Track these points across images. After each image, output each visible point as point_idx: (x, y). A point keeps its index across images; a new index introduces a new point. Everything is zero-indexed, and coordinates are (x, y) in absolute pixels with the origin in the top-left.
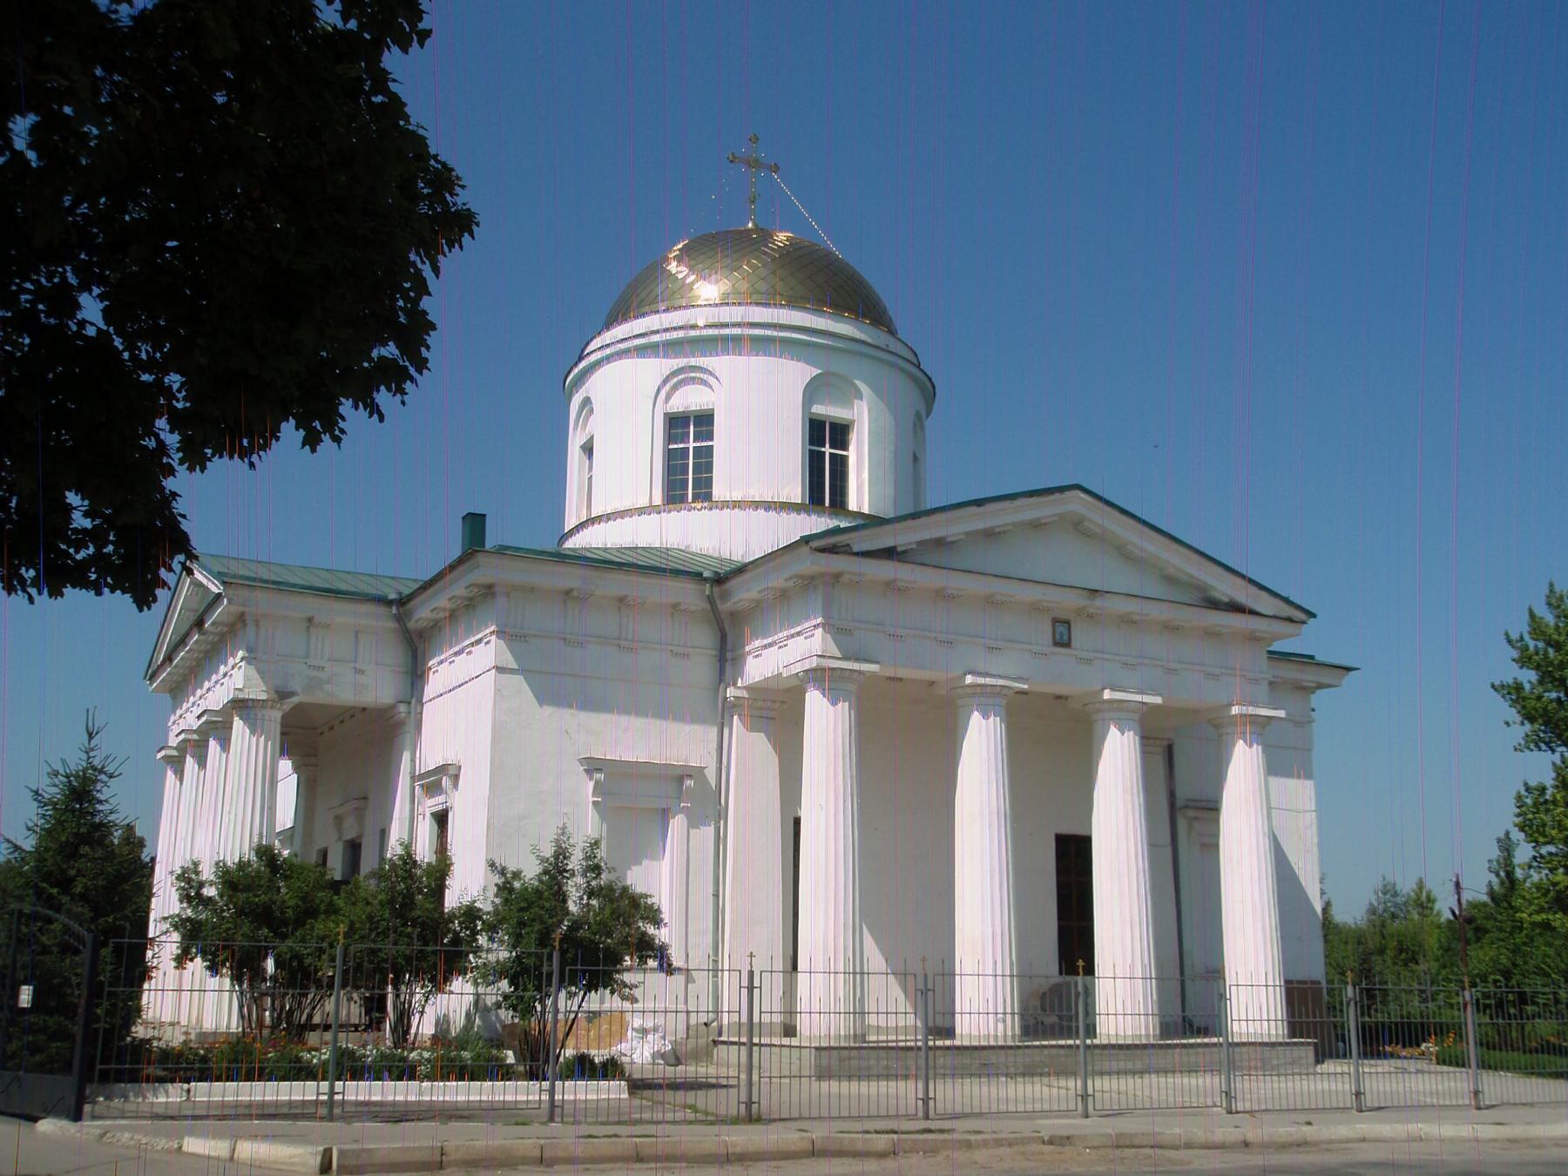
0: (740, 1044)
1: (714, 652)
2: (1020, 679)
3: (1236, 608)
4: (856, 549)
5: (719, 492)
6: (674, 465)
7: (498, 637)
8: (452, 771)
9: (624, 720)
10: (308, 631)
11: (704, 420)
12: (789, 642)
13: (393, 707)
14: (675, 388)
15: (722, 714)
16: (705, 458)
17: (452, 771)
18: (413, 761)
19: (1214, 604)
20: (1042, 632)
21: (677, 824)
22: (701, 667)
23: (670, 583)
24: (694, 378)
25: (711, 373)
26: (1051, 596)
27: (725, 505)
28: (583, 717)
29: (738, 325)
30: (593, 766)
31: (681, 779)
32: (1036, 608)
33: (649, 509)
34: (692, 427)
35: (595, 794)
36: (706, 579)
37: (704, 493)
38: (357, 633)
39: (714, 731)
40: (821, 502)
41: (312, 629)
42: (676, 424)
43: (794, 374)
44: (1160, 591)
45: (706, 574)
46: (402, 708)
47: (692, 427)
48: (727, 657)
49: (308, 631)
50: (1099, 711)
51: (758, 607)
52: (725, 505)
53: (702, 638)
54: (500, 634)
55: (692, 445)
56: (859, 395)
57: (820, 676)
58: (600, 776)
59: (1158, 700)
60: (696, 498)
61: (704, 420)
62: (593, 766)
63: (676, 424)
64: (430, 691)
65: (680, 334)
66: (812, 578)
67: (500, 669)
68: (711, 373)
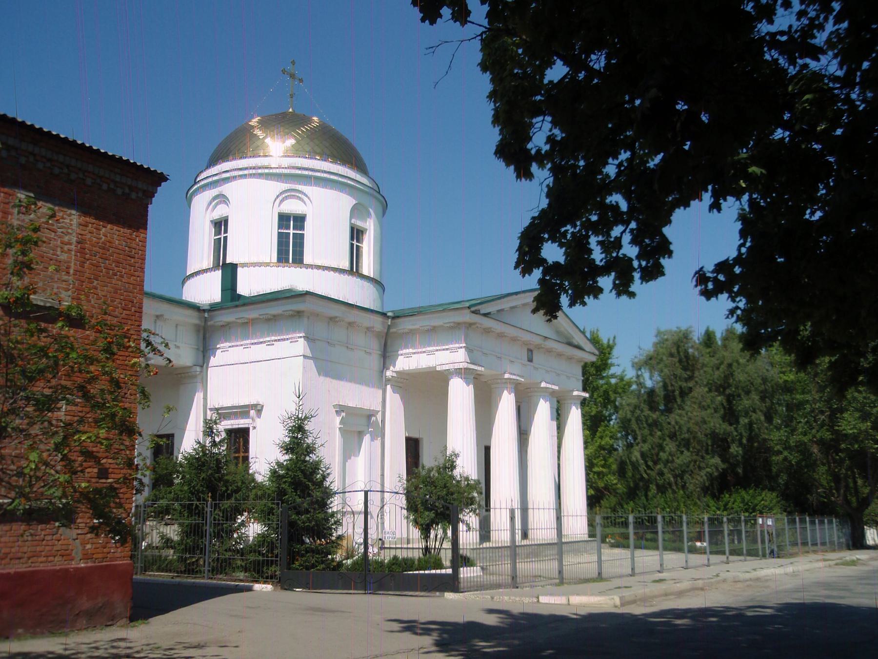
0: (419, 548)
1: (380, 353)
2: (522, 377)
3: (578, 347)
4: (482, 312)
5: (307, 260)
6: (282, 240)
7: (305, 340)
8: (259, 408)
9: (348, 385)
10: (155, 322)
11: (300, 220)
12: (436, 353)
13: (190, 367)
14: (286, 198)
15: (382, 382)
16: (299, 241)
17: (259, 408)
18: (205, 399)
19: (570, 344)
20: (524, 354)
21: (367, 438)
22: (374, 361)
23: (375, 318)
24: (298, 197)
25: (307, 196)
26: (527, 337)
27: (311, 266)
28: (335, 382)
29: (325, 172)
30: (340, 409)
31: (369, 417)
32: (525, 343)
33: (244, 265)
34: (292, 222)
35: (341, 423)
36: (388, 317)
37: (299, 260)
38: (530, 351)
39: (381, 392)
40: (287, 261)
41: (158, 321)
42: (284, 219)
43: (346, 202)
44: (554, 337)
45: (390, 314)
46: (198, 369)
47: (292, 222)
48: (386, 356)
49: (155, 322)
50: (536, 392)
51: (412, 332)
52: (311, 266)
53: (375, 346)
54: (306, 338)
55: (291, 231)
56: (369, 215)
57: (459, 372)
58: (343, 414)
59: (556, 388)
60: (294, 262)
61: (300, 220)
62: (340, 409)
63: (284, 219)
64: (213, 361)
65: (325, 175)
66: (459, 324)
67: (305, 357)
68: (307, 196)
